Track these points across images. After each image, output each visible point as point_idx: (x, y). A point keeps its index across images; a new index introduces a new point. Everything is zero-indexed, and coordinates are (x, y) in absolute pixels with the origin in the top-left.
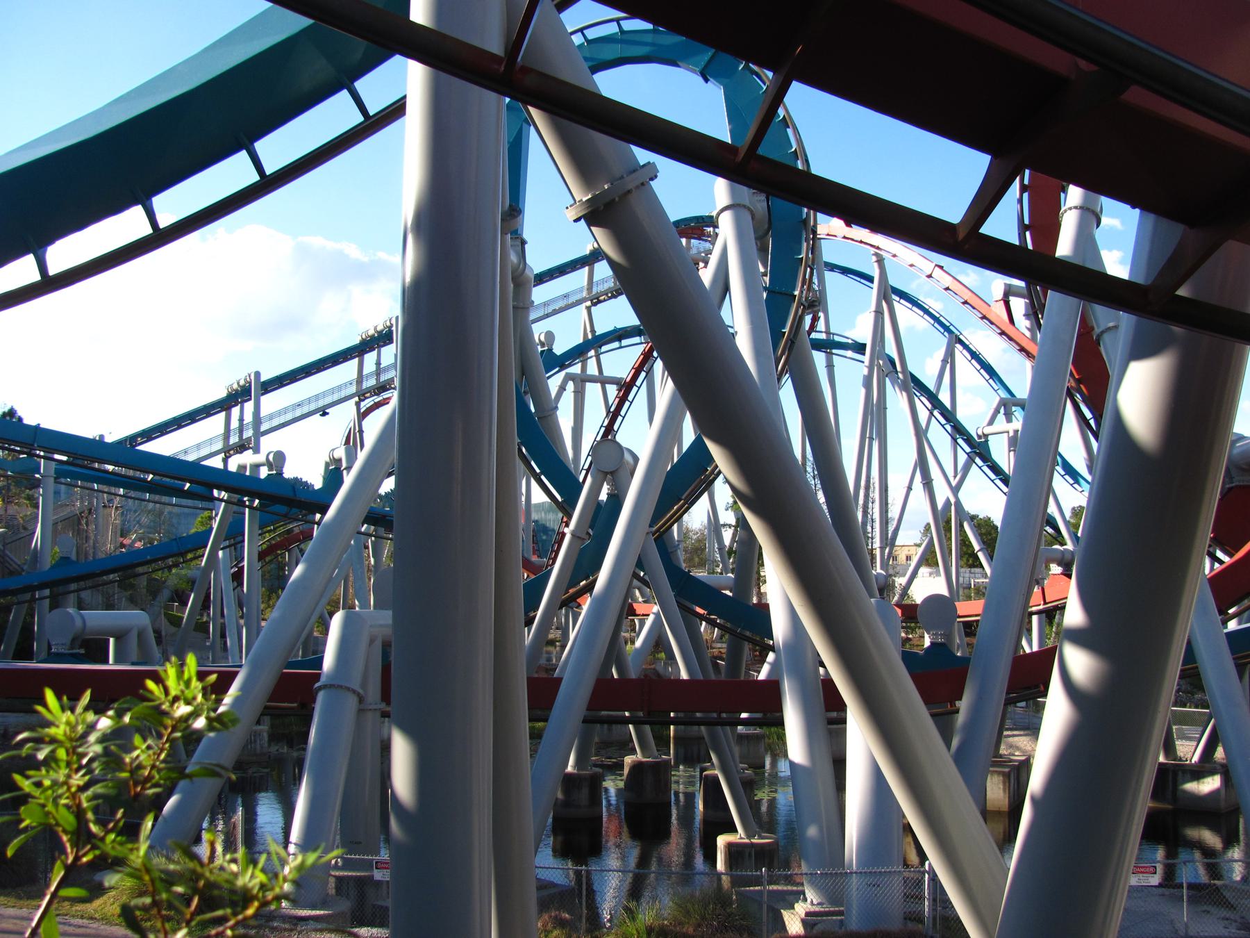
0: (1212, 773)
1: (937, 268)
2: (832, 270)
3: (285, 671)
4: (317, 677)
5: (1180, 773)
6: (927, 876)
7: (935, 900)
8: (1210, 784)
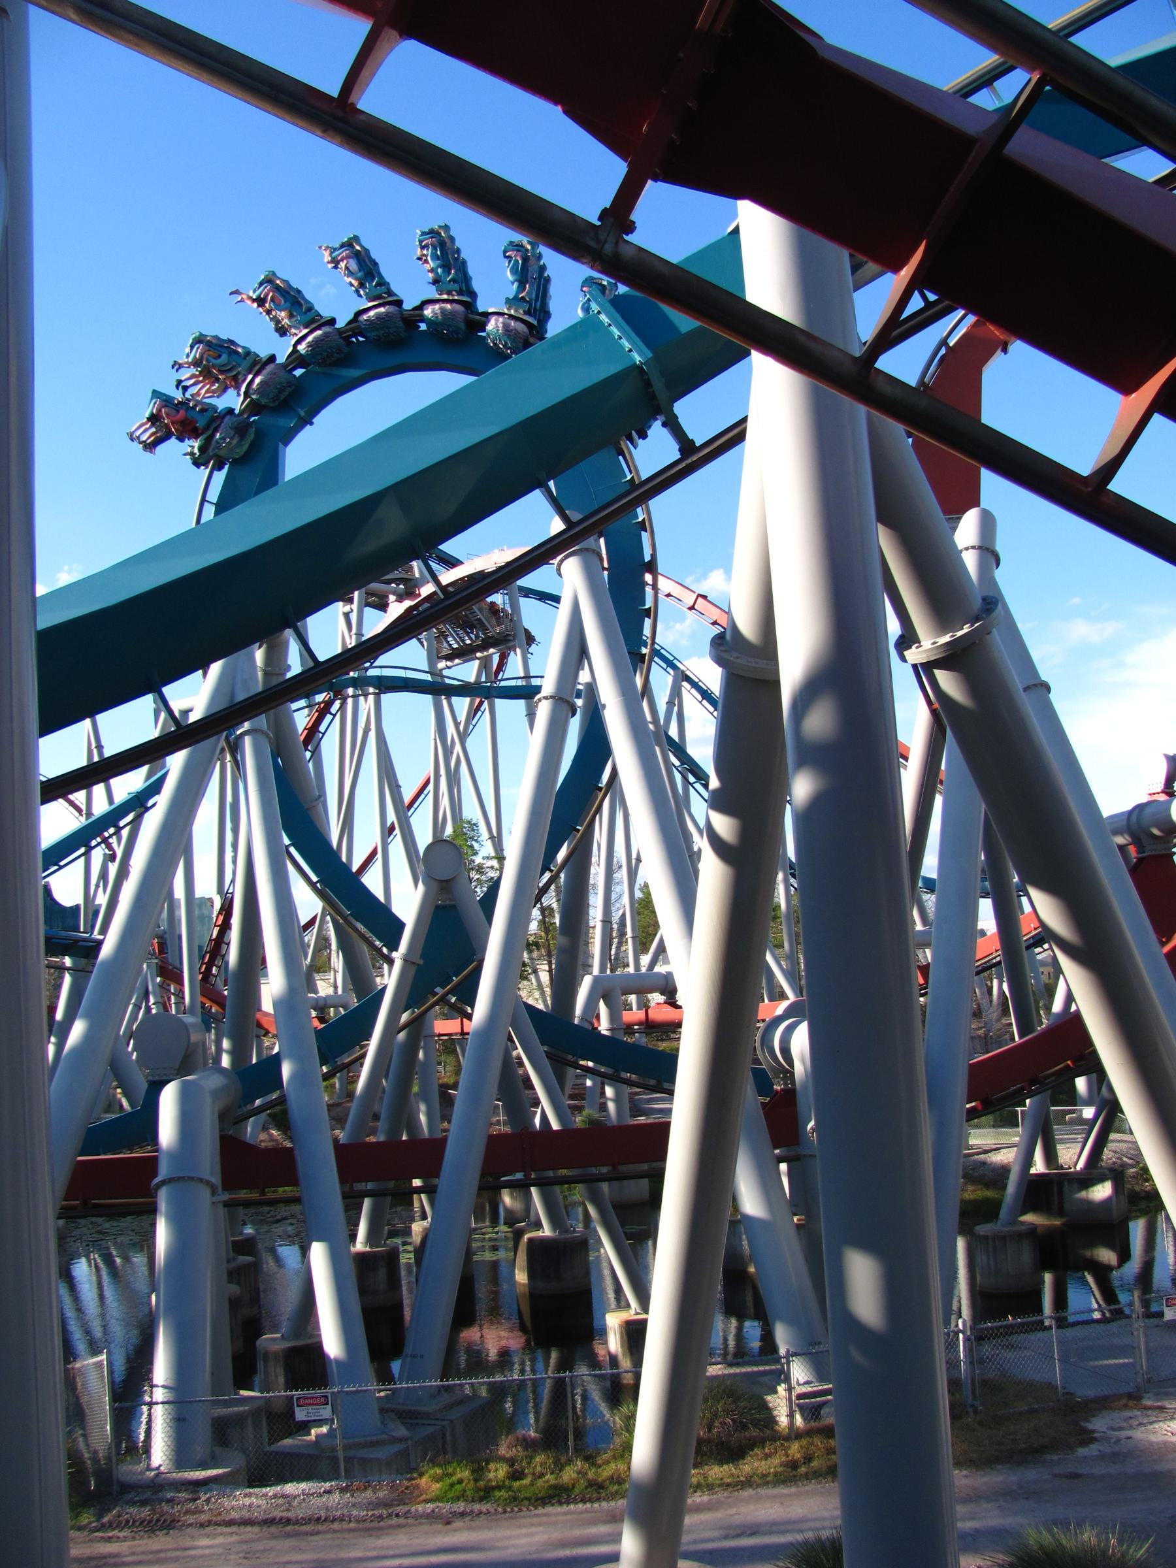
0: (1102, 1180)
1: (700, 599)
2: (526, 596)
3: (80, 1158)
4: (151, 1164)
5: (1066, 1183)
6: (961, 1336)
7: (972, 1363)
8: (1102, 1191)
